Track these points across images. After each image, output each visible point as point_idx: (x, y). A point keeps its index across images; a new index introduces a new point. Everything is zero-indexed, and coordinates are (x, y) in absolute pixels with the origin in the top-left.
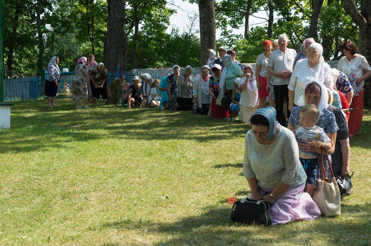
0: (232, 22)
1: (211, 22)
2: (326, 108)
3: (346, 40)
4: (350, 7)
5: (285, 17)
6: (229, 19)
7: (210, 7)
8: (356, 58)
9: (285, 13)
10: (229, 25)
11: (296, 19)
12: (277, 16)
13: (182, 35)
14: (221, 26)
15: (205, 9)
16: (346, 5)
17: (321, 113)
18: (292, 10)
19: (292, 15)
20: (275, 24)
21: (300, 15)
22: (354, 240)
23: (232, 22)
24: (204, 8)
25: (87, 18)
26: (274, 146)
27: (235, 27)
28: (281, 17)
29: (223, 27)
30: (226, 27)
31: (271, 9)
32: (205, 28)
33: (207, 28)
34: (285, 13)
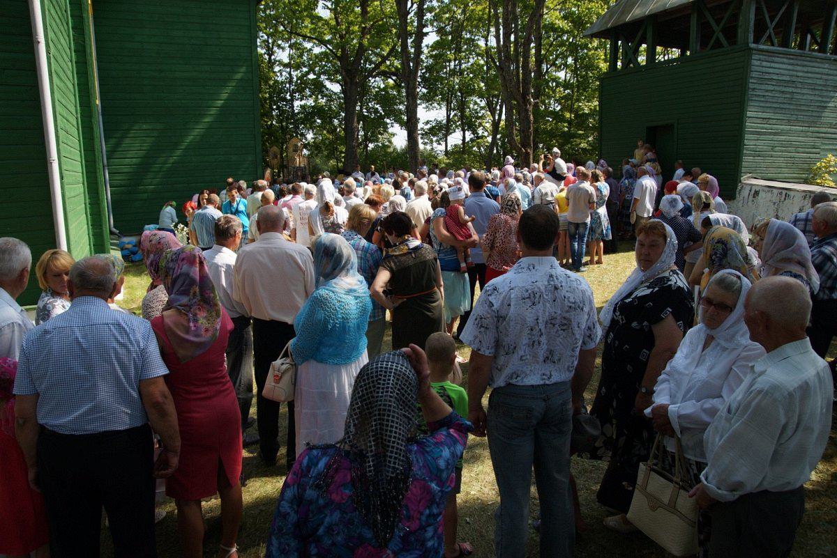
0: (437, 141)
2: (431, 211)
3: (269, 85)
6: (435, 139)
8: (821, 450)
9: (474, 132)
11: (482, 137)
12: (469, 136)
13: (441, 108)
17: (431, 61)
19: (480, 134)
20: (468, 142)
21: (486, 134)
23: (437, 141)
25: (332, 143)
26: (350, 385)
27: (440, 144)
28: (472, 136)
31: (464, 131)
34: (474, 132)
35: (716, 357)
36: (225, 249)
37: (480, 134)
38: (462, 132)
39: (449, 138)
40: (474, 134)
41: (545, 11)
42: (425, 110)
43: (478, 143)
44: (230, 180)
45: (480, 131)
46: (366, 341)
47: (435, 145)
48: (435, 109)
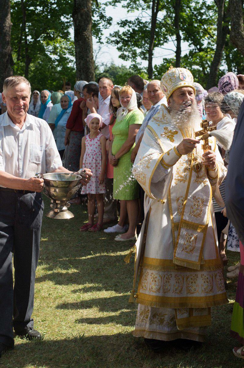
1: (88, 57)
4: (237, 38)
5: (197, 47)
6: (138, 51)
7: (87, 39)
9: (197, 42)
10: (139, 57)
14: (131, 58)
15: (81, 42)
16: (233, 36)
18: (205, 40)
22: (195, 205)
24: (79, 40)
28: (193, 47)
29: (132, 59)
30: (136, 59)
32: (81, 64)
33: (83, 64)
35: (177, 230)
36: (159, 258)
37: (205, 46)
38: (176, 42)
39: (157, 51)
40: (196, 46)
41: (212, 59)
42: (126, 9)
43: (201, 58)
44: (40, 199)
45: (205, 43)
46: (128, 253)
47: (139, 60)
48: (140, 9)
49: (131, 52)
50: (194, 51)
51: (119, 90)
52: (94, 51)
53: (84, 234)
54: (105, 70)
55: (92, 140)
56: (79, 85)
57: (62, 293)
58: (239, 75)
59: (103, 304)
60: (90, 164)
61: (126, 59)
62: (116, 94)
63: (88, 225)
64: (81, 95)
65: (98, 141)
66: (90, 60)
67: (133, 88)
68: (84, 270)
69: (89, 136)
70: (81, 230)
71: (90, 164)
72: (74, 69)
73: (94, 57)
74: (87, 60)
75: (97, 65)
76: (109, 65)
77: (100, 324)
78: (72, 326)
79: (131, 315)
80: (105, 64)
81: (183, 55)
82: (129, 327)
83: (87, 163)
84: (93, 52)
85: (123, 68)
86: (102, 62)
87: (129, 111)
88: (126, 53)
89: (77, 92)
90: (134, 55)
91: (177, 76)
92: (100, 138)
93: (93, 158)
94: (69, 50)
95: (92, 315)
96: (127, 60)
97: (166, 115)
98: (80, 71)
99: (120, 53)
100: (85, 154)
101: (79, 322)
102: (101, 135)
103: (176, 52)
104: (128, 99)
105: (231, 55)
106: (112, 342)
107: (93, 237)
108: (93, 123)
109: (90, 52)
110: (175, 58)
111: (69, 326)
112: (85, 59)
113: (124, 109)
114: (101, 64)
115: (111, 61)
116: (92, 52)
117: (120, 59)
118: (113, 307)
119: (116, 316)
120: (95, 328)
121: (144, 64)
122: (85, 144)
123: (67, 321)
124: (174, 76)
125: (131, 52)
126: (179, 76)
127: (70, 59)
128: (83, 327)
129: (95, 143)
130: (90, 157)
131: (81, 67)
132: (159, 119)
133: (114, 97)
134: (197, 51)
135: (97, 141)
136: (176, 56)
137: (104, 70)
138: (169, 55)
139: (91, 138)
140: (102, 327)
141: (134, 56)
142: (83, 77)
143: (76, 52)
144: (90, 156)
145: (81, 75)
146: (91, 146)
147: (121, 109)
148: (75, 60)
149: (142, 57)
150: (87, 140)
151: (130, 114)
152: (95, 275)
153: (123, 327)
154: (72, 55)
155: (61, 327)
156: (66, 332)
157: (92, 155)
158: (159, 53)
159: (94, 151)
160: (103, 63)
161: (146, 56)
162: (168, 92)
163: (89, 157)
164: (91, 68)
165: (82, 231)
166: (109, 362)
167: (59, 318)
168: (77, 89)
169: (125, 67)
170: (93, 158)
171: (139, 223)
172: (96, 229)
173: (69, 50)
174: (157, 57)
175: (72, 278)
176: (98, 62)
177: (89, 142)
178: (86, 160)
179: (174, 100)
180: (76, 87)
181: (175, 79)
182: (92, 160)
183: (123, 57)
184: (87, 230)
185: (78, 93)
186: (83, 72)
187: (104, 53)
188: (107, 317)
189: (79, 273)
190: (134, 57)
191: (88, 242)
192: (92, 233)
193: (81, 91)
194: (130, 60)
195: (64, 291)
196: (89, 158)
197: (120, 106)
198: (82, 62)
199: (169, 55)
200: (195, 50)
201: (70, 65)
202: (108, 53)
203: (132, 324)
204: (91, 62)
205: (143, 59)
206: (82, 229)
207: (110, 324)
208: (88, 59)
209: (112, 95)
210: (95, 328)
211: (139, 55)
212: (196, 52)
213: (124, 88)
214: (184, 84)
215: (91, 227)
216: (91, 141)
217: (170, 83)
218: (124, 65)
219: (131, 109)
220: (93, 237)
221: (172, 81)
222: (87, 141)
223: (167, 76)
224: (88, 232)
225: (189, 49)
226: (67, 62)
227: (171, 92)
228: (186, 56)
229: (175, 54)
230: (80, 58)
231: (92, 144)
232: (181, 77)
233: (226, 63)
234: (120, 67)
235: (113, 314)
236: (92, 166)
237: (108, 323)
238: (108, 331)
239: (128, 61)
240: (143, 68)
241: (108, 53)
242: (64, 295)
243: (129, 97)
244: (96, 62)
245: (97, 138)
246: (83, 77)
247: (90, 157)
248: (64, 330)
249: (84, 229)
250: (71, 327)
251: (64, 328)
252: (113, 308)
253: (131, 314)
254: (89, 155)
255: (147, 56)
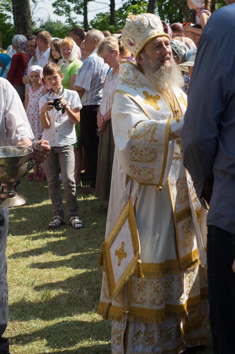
1: (25, 12)
14: (65, 13)
29: (67, 13)
30: (70, 14)
33: (21, 19)
47: (73, 14)
49: (65, 7)
50: (128, 4)
51: (58, 43)
52: (30, 7)
53: (30, 183)
54: (41, 26)
55: (35, 92)
56: (16, 39)
57: (12, 241)
58: (171, 25)
59: (52, 248)
60: (32, 115)
61: (60, 14)
62: (57, 47)
63: (33, 175)
64: (20, 49)
65: (41, 93)
66: (28, 16)
67: (74, 40)
68: (32, 218)
69: (32, 88)
70: (26, 179)
71: (32, 115)
72: (11, 25)
73: (31, 13)
74: (24, 15)
75: (33, 21)
76: (45, 20)
77: (50, 268)
78: (24, 272)
79: (80, 259)
80: (41, 19)
81: (117, 8)
82: (79, 270)
83: (30, 115)
84: (30, 8)
85: (59, 23)
86: (39, 17)
87: (70, 62)
88: (61, 9)
89: (15, 47)
90: (68, 9)
91: (146, 23)
92: (42, 90)
93: (36, 110)
94: (6, 6)
95: (43, 261)
96: (61, 15)
97: (139, 76)
98: (18, 26)
99: (55, 9)
100: (28, 106)
101: (31, 267)
102: (43, 87)
103: (110, 6)
104: (69, 51)
105: (163, 6)
106: (63, 285)
107: (39, 186)
108: (32, 76)
109: (27, 7)
110: (109, 11)
111: (21, 272)
112: (23, 15)
113: (65, 60)
114: (38, 20)
115: (47, 16)
116: (28, 8)
117: (54, 14)
118: (62, 251)
119: (66, 260)
120: (46, 273)
121: (80, 18)
122: (28, 96)
123: (18, 267)
124: (143, 25)
125: (65, 7)
126: (149, 24)
127: (7, 16)
128: (34, 272)
129: (38, 95)
130: (32, 109)
131: (18, 22)
132: (131, 81)
133: (54, 50)
134: (130, 3)
135: (40, 93)
136: (111, 10)
137: (40, 26)
138: (103, 8)
139: (33, 89)
140: (53, 271)
141: (67, 10)
142: (21, 31)
143: (13, 8)
144: (32, 107)
145: (19, 30)
146: (34, 98)
147: (62, 60)
148: (12, 16)
149: (76, 11)
150: (30, 92)
151: (71, 65)
152: (43, 222)
153: (74, 270)
154: (9, 11)
155: (13, 273)
156: (18, 278)
157: (35, 106)
158: (93, 7)
159: (37, 102)
160: (39, 19)
161: (80, 10)
162: (137, 45)
163: (31, 108)
164: (29, 23)
165: (28, 180)
166: (61, 305)
167: (10, 265)
168: (15, 44)
169: (60, 22)
170: (36, 110)
171: (86, 172)
172: (41, 178)
173: (6, 6)
174: (92, 11)
175: (21, 226)
176: (35, 18)
177: (31, 93)
178: (28, 112)
179: (147, 56)
180: (14, 41)
181: (140, 28)
182: (35, 112)
183: (58, 13)
184: (32, 179)
185: (16, 48)
186: (21, 27)
187: (40, 8)
188: (57, 262)
189: (27, 221)
190: (68, 12)
191: (34, 191)
192: (37, 182)
193: (19, 46)
194: (64, 15)
195: (13, 239)
196: (31, 110)
197: (61, 58)
198: (20, 17)
199: (103, 8)
200: (129, 3)
201: (7, 21)
202: (44, 8)
203: (81, 267)
204: (28, 17)
205: (77, 13)
206: (27, 179)
207: (60, 268)
208: (25, 14)
209: (52, 48)
210: (46, 273)
211: (73, 10)
212: (129, 5)
213: (66, 40)
214: (158, 32)
215: (37, 176)
216: (33, 93)
217: (139, 33)
218: (59, 20)
219: (72, 60)
220: (38, 186)
221: (141, 30)
222: (30, 93)
223: (133, 25)
224: (33, 181)
225: (122, 3)
226: (5, 18)
227: (142, 45)
228: (120, 9)
229: (109, 8)
230: (17, 14)
231: (34, 96)
232: (152, 24)
233: (159, 15)
234: (56, 22)
235: (62, 258)
236: (34, 118)
237: (59, 267)
238: (59, 274)
239: (62, 16)
240: (78, 22)
241: (44, 8)
242: (14, 243)
243: (69, 49)
244: (33, 18)
245: (39, 89)
246: (21, 31)
247: (32, 109)
248: (16, 276)
249: (30, 179)
250: (22, 273)
251: (16, 273)
252: (62, 253)
253: (80, 258)
254: (31, 106)
255: (82, 11)
